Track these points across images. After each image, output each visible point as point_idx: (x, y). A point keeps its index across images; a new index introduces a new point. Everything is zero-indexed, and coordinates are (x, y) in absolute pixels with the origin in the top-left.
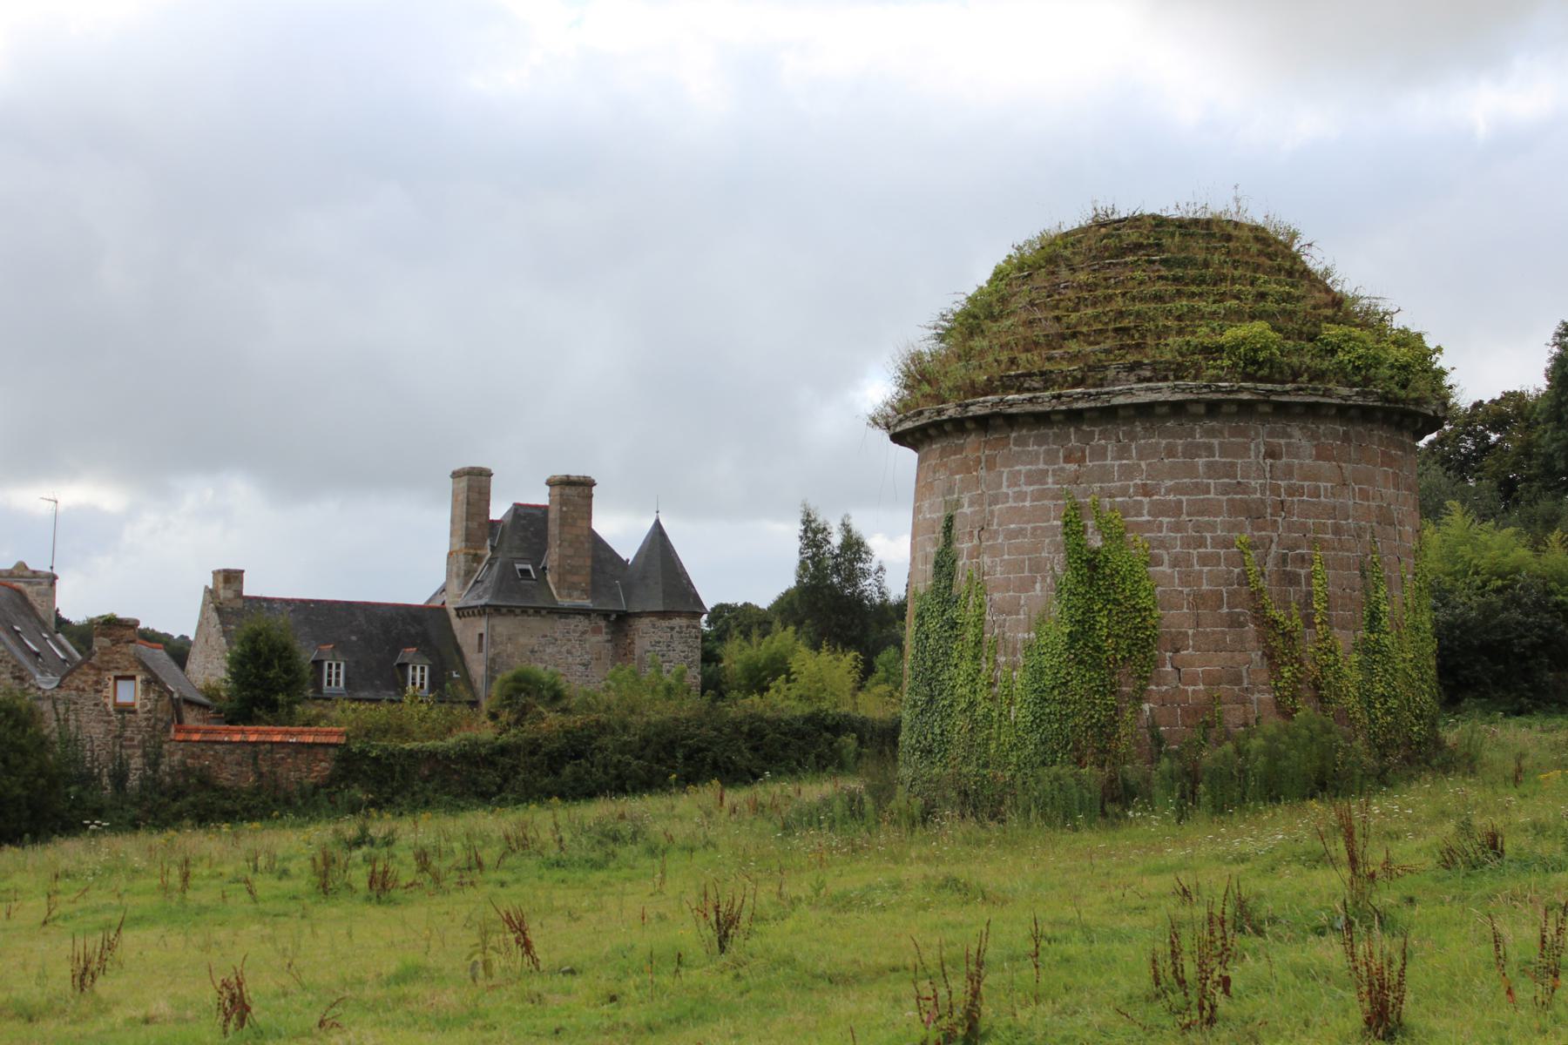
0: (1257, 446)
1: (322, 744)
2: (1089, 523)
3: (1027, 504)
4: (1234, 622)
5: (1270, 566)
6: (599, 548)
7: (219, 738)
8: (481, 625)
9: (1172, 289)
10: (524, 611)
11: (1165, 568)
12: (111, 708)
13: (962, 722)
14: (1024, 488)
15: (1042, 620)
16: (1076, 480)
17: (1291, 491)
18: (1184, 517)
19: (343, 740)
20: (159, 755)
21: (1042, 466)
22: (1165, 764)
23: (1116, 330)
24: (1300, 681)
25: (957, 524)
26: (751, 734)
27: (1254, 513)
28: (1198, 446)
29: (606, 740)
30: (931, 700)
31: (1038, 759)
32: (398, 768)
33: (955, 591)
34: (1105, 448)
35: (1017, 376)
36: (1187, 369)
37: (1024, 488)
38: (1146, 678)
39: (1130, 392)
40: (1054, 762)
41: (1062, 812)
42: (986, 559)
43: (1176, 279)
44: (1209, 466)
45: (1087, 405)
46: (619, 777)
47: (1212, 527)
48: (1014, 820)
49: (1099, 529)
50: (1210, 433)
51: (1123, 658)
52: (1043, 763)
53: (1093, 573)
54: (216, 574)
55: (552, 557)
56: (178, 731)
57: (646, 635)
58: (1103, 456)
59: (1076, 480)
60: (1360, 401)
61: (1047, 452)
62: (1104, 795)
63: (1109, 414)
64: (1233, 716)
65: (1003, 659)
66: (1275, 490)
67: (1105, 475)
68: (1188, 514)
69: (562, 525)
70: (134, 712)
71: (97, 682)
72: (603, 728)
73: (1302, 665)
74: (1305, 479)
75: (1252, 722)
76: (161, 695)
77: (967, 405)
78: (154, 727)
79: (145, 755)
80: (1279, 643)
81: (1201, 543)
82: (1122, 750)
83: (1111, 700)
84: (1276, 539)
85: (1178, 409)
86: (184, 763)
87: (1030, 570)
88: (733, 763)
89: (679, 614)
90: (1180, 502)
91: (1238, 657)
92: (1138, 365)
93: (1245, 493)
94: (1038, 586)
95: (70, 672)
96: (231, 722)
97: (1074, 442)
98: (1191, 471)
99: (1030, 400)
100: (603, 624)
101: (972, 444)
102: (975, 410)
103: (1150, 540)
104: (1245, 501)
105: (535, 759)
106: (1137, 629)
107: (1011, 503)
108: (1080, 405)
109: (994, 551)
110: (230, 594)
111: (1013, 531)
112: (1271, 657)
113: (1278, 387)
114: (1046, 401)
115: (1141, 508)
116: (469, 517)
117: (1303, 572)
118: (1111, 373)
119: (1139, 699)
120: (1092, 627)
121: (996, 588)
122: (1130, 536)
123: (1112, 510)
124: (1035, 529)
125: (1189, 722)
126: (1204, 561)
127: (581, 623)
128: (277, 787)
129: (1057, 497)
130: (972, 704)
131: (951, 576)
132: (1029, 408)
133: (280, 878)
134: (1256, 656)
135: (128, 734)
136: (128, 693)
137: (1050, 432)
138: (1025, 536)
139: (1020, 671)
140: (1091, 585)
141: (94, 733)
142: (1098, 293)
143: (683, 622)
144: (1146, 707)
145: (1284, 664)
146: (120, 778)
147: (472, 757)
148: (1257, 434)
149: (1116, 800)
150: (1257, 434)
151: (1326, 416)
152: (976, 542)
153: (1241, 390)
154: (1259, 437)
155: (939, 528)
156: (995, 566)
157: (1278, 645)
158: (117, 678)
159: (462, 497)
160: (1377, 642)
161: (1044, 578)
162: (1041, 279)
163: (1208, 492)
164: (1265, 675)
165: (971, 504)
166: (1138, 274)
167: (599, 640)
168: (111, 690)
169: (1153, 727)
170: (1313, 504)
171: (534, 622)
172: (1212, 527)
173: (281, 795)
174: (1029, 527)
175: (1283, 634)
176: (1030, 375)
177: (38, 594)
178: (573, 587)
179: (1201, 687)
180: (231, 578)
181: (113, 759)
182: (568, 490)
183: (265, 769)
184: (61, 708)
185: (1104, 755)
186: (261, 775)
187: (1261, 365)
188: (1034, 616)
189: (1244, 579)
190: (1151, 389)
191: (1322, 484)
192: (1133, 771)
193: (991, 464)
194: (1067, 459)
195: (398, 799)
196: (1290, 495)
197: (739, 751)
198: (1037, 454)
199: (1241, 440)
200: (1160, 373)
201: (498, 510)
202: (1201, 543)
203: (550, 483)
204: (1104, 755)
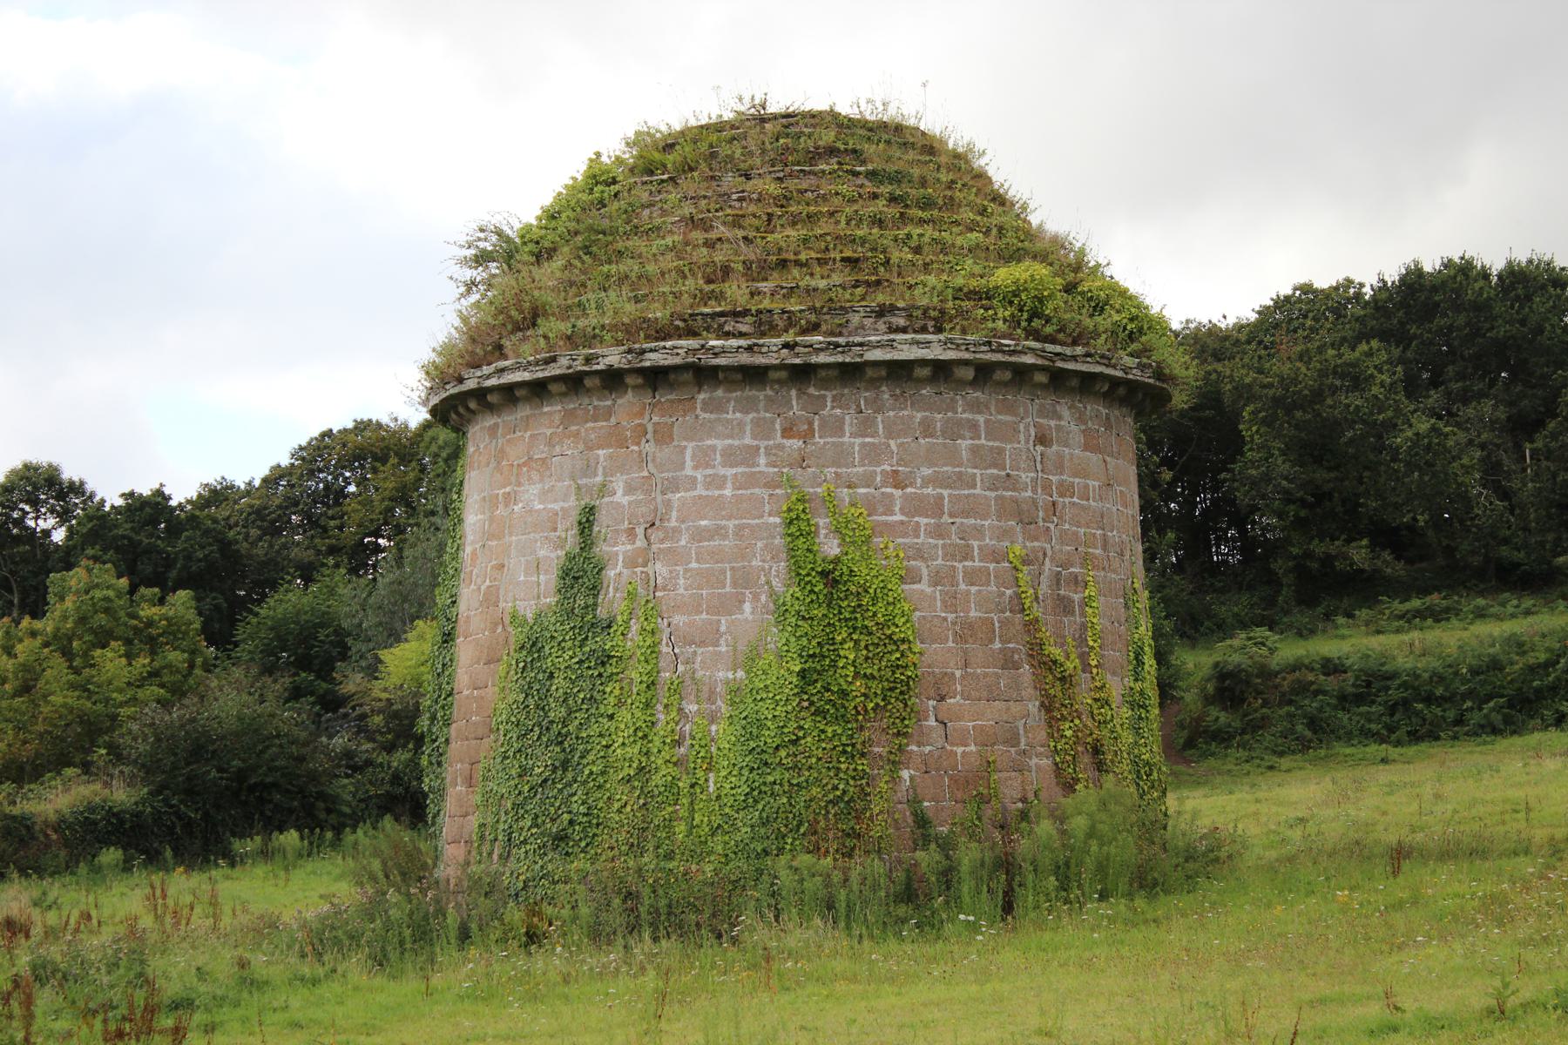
0: (1027, 428)
2: (821, 522)
3: (728, 492)
4: (1009, 663)
5: (1044, 589)
11: (924, 586)
14: (722, 471)
16: (802, 462)
17: (1066, 490)
18: (946, 519)
21: (748, 441)
28: (959, 423)
33: (602, 613)
34: (841, 421)
35: (714, 315)
38: (905, 735)
39: (890, 344)
40: (781, 851)
44: (975, 450)
45: (831, 359)
47: (979, 532)
48: (757, 933)
50: (976, 407)
53: (833, 596)
58: (840, 431)
59: (802, 462)
61: (757, 423)
63: (851, 373)
64: (1010, 789)
66: (1047, 487)
67: (841, 457)
68: (951, 516)
75: (1031, 796)
77: (643, 352)
80: (1056, 690)
81: (967, 556)
84: (1049, 553)
85: (941, 371)
87: (735, 584)
90: (941, 497)
91: (1015, 708)
92: (892, 309)
93: (1014, 490)
94: (747, 607)
97: (796, 409)
98: (953, 457)
99: (749, 349)
101: (627, 406)
102: (653, 359)
103: (905, 547)
104: (1016, 501)
107: (700, 491)
109: (674, 557)
113: (1068, 351)
114: (772, 351)
115: (892, 502)
117: (1076, 597)
119: (896, 765)
121: (677, 608)
123: (853, 505)
124: (740, 528)
125: (959, 795)
126: (972, 577)
129: (771, 484)
132: (745, 359)
133: (1396, 872)
134: (1033, 707)
137: (761, 395)
138: (725, 537)
139: (724, 724)
144: (905, 774)
145: (1063, 718)
150: (1026, 411)
152: (640, 543)
156: (678, 579)
163: (974, 486)
164: (1044, 734)
165: (629, 490)
169: (914, 802)
170: (1083, 508)
172: (979, 532)
175: (1063, 679)
176: (736, 314)
179: (973, 748)
190: (918, 343)
191: (1091, 483)
193: (664, 436)
194: (788, 432)
196: (1062, 495)
198: (741, 424)
199: (1008, 418)
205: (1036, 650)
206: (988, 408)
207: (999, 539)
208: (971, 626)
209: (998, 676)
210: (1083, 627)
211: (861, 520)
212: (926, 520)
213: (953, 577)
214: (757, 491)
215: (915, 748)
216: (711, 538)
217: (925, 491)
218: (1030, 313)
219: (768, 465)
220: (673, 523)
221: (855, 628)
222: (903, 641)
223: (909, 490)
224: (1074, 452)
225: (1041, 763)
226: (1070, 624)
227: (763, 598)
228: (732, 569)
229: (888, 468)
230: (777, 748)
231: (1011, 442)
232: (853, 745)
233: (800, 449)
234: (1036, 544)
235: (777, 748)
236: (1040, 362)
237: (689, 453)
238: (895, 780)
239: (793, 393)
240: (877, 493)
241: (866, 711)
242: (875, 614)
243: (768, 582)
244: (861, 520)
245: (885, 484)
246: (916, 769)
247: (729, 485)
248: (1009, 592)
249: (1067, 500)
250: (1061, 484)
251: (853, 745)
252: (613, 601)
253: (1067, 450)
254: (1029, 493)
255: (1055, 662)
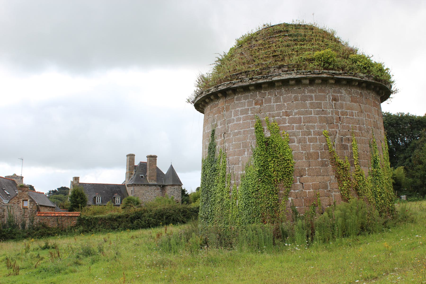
0: (329, 96)
1: (74, 216)
2: (265, 128)
3: (241, 122)
4: (324, 164)
5: (336, 142)
6: (158, 171)
7: (48, 215)
8: (132, 188)
9: (293, 43)
10: (141, 185)
11: (296, 144)
12: (21, 208)
13: (218, 207)
14: (240, 116)
15: (248, 166)
16: (260, 112)
18: (302, 124)
19: (79, 215)
20: (33, 220)
21: (246, 107)
22: (300, 222)
23: (273, 56)
24: (350, 187)
25: (216, 133)
26: (183, 212)
27: (329, 122)
29: (146, 214)
30: (207, 199)
31: (247, 221)
32: (93, 222)
33: (216, 158)
36: (301, 66)
37: (240, 116)
39: (280, 75)
40: (254, 222)
41: (257, 246)
42: (227, 144)
43: (294, 40)
44: (311, 104)
45: (263, 81)
46: (148, 223)
47: (313, 127)
49: (269, 129)
50: (311, 91)
51: (280, 180)
52: (249, 222)
53: (268, 148)
54: (73, 178)
55: (148, 174)
56: (38, 213)
57: (169, 190)
58: (270, 102)
59: (260, 112)
60: (366, 79)
61: (248, 102)
62: (274, 235)
63: (272, 85)
64: (325, 202)
65: (233, 182)
66: (337, 113)
67: (271, 109)
68: (304, 123)
69: (150, 166)
70: (27, 209)
71: (18, 201)
72: (145, 211)
73: (350, 181)
74: (347, 110)
75: (332, 204)
76: (34, 204)
77: (218, 87)
78: (32, 213)
79: (30, 220)
80: (341, 172)
81: (309, 134)
82: (281, 216)
83: (275, 196)
84: (338, 132)
85: (298, 81)
86: (39, 221)
87: (243, 147)
88: (178, 219)
89: (176, 185)
90: (301, 118)
92: (283, 66)
93: (325, 114)
94: (246, 153)
95: (11, 199)
96: (69, 211)
97: (258, 97)
98: (305, 106)
100: (159, 188)
101: (221, 103)
104: (326, 117)
105: (127, 219)
106: (285, 168)
107: (235, 122)
108: (260, 81)
110: (76, 182)
111: (236, 133)
112: (338, 178)
113: (337, 72)
116: (130, 165)
117: (349, 145)
118: (272, 70)
119: (287, 196)
120: (267, 168)
122: (281, 132)
123: (274, 122)
124: (244, 131)
125: (307, 204)
126: (311, 140)
127: (154, 188)
128: (63, 227)
129: (252, 118)
130: (222, 200)
131: (214, 152)
134: (333, 177)
135: (26, 214)
136: (27, 204)
138: (241, 134)
140: (267, 151)
141: (17, 214)
142: (266, 46)
143: (177, 187)
144: (290, 199)
145: (344, 180)
146: (24, 226)
147: (112, 219)
148: (329, 92)
149: (280, 237)
151: (354, 86)
152: (223, 138)
153: (322, 73)
154: (330, 92)
155: (210, 135)
157: (341, 172)
158: (23, 200)
159: (128, 160)
160: (377, 172)
161: (248, 150)
162: (246, 46)
163: (311, 114)
164: (337, 185)
165: (221, 125)
166: (280, 39)
167: (158, 191)
168: (22, 203)
169: (293, 207)
170: (351, 119)
171: (144, 187)
172: (313, 127)
173: (63, 229)
174: (242, 131)
175: (343, 169)
177: (18, 181)
178: (152, 179)
179: (312, 190)
180: (76, 179)
181: (22, 220)
182: (151, 158)
183: (60, 223)
184: (9, 208)
185: (274, 219)
186: (59, 224)
187: (330, 64)
188: (245, 164)
189: (327, 147)
192: (286, 226)
193: (227, 109)
194: (256, 104)
195: (92, 230)
197: (180, 216)
198: (245, 103)
199: (323, 94)
200: (291, 68)
201: (137, 163)
202: (309, 134)
203: (147, 157)
204: (274, 219)
205: (333, 161)
206: (316, 92)
207: (320, 129)
208: (311, 154)
209: (320, 169)
210: (352, 153)
211: (276, 126)
212: (296, 125)
213: (305, 140)
214: (248, 121)
215: (293, 191)
216: (237, 135)
217: (296, 116)
218: (326, 63)
219: (251, 113)
220: (229, 132)
221: (274, 157)
222: (288, 160)
223: (290, 116)
224: (347, 102)
225: (336, 194)
226: (346, 153)
227: (250, 150)
228: (242, 143)
229: (284, 111)
230: (253, 192)
231: (324, 101)
232: (273, 191)
233: (259, 108)
234: (333, 129)
235: (253, 192)
236: (328, 76)
237: (233, 112)
238: (287, 201)
239: (258, 93)
240: (281, 118)
241: (277, 180)
242: (280, 153)
243: (251, 146)
244: (276, 126)
245: (283, 115)
246: (293, 197)
247: (242, 120)
248: (324, 144)
249: (345, 117)
250: (342, 112)
251: (273, 191)
252: (218, 154)
253: (344, 102)
254: (331, 115)
255: (340, 164)
